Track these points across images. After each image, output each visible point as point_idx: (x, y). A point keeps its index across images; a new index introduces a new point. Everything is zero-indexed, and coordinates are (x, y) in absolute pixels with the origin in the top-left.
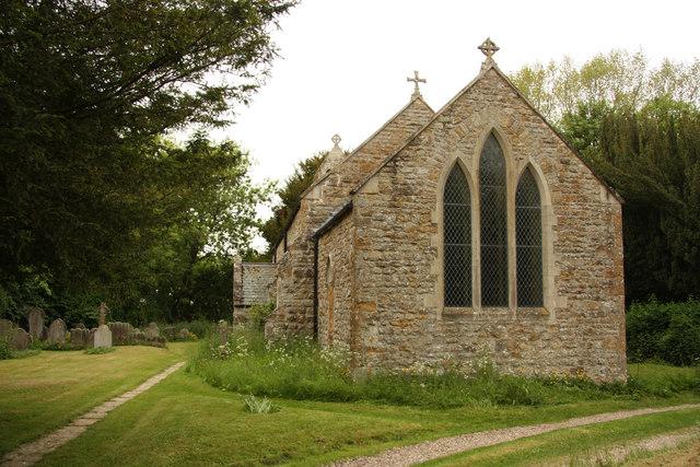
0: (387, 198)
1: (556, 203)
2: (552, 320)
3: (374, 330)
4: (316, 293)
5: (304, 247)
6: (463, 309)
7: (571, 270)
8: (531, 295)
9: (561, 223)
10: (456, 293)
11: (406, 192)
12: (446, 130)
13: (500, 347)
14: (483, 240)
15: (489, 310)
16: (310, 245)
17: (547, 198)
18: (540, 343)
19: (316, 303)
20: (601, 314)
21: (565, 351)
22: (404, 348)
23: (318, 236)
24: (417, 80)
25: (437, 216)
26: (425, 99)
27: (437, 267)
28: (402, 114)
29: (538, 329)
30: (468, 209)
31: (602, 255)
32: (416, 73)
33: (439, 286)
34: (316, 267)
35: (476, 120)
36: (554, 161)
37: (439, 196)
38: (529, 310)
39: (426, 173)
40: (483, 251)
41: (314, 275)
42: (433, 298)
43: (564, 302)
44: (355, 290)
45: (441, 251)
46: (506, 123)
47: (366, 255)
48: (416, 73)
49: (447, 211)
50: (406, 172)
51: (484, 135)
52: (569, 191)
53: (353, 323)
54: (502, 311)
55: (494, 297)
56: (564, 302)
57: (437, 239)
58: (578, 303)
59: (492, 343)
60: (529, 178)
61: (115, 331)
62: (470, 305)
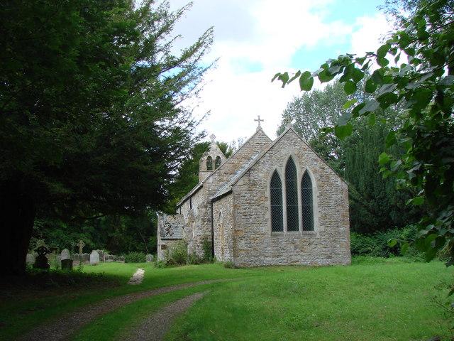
0: (247, 187)
1: (319, 186)
2: (318, 236)
3: (243, 242)
4: (213, 229)
5: (206, 207)
6: (280, 233)
7: (325, 215)
8: (308, 226)
9: (321, 194)
10: (276, 226)
11: (254, 184)
12: (271, 156)
13: (296, 248)
14: (288, 203)
15: (292, 233)
16: (209, 206)
17: (314, 184)
18: (313, 246)
19: (213, 233)
20: (339, 233)
21: (324, 249)
22: (255, 249)
23: (213, 201)
24: (259, 120)
25: (268, 194)
26: (263, 130)
27: (268, 215)
28: (252, 138)
29: (312, 240)
30: (296, 182)
31: (339, 208)
32: (259, 116)
33: (269, 223)
34: (212, 216)
35: (284, 152)
36: (318, 168)
37: (269, 185)
38: (307, 232)
39: (263, 176)
40: (303, 207)
41: (211, 220)
42: (267, 228)
43: (323, 228)
44: (235, 226)
45: (269, 208)
46: (296, 152)
47: (239, 211)
48: (259, 116)
49: (272, 192)
50: (254, 175)
51: (287, 158)
52: (324, 180)
53: (234, 239)
54: (297, 233)
55: (292, 226)
56: (323, 228)
57: (268, 203)
58: (329, 229)
59: (292, 246)
60: (306, 177)
61: (101, 255)
62: (282, 230)
